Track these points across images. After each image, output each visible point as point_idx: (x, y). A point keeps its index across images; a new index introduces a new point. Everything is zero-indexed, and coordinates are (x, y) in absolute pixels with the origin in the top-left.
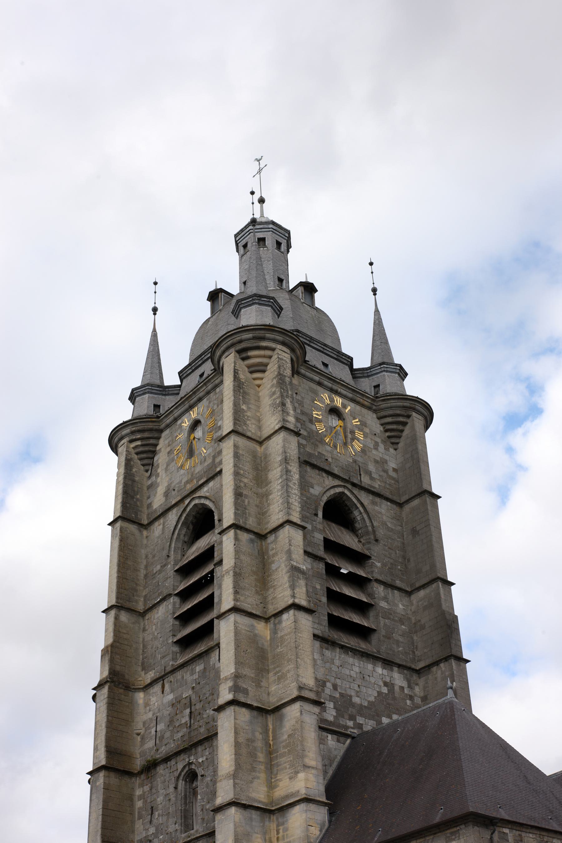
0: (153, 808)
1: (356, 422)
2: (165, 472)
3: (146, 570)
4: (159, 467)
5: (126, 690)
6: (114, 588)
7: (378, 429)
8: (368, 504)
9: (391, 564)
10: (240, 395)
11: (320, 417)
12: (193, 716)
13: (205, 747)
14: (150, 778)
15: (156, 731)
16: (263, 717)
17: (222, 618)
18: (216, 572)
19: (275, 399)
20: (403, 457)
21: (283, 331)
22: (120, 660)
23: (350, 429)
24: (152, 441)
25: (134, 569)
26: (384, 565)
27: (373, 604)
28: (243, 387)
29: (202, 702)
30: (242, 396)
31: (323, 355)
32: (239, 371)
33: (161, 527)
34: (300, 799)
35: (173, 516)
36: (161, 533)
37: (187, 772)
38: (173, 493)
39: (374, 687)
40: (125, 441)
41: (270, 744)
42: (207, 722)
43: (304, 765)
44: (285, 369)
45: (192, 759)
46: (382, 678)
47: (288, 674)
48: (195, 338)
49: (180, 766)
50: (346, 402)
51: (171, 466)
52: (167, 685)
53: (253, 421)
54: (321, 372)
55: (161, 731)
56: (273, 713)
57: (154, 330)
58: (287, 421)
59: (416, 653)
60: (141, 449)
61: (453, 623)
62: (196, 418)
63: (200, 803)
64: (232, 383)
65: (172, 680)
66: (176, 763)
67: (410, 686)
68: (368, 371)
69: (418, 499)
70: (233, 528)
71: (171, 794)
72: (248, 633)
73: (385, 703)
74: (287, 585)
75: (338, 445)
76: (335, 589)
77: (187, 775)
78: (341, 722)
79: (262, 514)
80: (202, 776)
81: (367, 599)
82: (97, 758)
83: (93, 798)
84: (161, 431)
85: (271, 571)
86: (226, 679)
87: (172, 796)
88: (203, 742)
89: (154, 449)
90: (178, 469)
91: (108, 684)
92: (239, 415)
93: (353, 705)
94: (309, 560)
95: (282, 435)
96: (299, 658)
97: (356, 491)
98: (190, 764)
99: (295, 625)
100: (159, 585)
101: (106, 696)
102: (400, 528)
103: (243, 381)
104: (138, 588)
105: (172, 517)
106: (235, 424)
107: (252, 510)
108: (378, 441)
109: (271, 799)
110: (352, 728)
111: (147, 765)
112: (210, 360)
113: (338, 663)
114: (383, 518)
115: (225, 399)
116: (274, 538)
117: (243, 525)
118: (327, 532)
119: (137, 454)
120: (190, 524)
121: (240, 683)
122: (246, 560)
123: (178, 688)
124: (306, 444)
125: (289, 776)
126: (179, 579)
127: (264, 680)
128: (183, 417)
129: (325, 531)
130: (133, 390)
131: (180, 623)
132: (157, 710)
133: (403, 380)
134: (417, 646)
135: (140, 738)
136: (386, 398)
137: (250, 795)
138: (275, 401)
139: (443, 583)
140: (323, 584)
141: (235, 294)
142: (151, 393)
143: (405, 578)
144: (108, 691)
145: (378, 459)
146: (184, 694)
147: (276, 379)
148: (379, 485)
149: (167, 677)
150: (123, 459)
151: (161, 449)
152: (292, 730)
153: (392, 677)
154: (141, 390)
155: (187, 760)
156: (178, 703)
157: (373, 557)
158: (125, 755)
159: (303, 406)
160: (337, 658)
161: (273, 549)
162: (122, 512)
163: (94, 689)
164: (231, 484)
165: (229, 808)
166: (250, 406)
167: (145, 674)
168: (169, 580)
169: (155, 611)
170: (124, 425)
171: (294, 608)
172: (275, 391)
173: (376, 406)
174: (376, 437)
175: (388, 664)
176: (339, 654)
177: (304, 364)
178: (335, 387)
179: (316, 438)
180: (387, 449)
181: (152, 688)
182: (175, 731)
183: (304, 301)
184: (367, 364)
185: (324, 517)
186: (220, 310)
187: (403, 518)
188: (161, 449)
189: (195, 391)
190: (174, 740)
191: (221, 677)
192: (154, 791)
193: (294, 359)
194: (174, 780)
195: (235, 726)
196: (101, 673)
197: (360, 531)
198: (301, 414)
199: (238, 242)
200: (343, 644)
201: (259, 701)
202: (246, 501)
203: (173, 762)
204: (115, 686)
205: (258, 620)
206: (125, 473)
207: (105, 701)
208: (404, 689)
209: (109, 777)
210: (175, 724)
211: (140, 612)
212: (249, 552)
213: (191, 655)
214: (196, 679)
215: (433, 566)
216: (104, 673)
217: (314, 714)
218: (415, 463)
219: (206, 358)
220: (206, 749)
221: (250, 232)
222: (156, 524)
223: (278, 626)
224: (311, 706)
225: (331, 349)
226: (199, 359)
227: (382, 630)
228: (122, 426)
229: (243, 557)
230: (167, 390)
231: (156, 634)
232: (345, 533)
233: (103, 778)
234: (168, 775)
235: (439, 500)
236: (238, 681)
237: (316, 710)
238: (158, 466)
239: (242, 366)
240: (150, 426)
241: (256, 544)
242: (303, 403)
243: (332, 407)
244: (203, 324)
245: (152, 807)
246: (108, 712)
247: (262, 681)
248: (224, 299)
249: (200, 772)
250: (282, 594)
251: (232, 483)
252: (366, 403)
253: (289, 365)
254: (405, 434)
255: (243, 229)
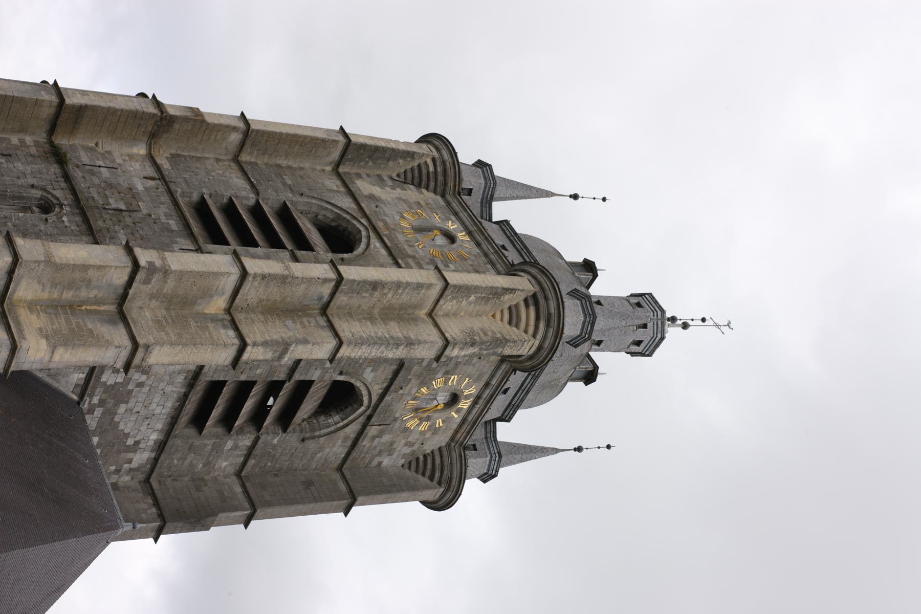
0: (9, 157)
1: (439, 423)
2: (397, 198)
3: (286, 167)
4: (403, 190)
5: (150, 135)
6: (270, 129)
7: (428, 448)
8: (346, 432)
9: (275, 455)
10: (486, 294)
11: (450, 383)
12: (117, 212)
13: (81, 226)
14: (45, 155)
15: (100, 166)
16: (115, 299)
17: (235, 258)
18: (283, 252)
19: (479, 334)
20: (393, 474)
21: (555, 348)
22: (186, 130)
23: (432, 416)
24: (432, 184)
25: (288, 153)
26: (274, 447)
27: (232, 433)
28: (494, 298)
29: (133, 225)
30: (485, 297)
31: (517, 389)
32: (514, 295)
33: (335, 188)
34: (15, 340)
35: (348, 204)
36: (328, 188)
37: (51, 201)
38: (373, 206)
39: (135, 429)
40: (435, 153)
41: (81, 306)
42: (110, 230)
43: (56, 347)
44: (511, 348)
45: (67, 209)
46: (144, 440)
47: (164, 333)
48: (544, 241)
49: (58, 193)
50: (463, 413)
51: (403, 205)
52: (154, 184)
53: (455, 307)
54: (500, 387)
55: (100, 172)
56: (119, 312)
57: (553, 195)
58: (454, 348)
59: (169, 479)
60: (424, 171)
61: (202, 525)
62: (458, 239)
63: (14, 215)
64: (500, 286)
65: (159, 190)
66: (62, 189)
67: (131, 470)
68: (492, 438)
69: (346, 491)
70: (338, 277)
71: (26, 180)
72: (215, 288)
73: (115, 441)
74: (268, 338)
75: (416, 402)
76: (253, 390)
77: (48, 201)
78: (98, 390)
79: (350, 314)
80: (46, 220)
81: (237, 426)
82: (73, 93)
83: (26, 85)
84: (443, 196)
85: (284, 319)
86: (163, 259)
87: (23, 181)
88: (86, 223)
89: (423, 185)
90: (400, 213)
91: (159, 114)
92: (464, 292)
93: (117, 405)
94: (290, 363)
95: (440, 343)
96: (182, 348)
97: (362, 419)
98: (61, 206)
99: (221, 345)
100: (269, 181)
101: (145, 110)
102: (314, 467)
103: (502, 299)
104: (266, 156)
105: (346, 203)
106: (455, 286)
107: (355, 301)
108: (415, 447)
109: (17, 304)
110: (90, 402)
111: (60, 153)
112: (523, 261)
113: (167, 390)
114: (327, 448)
115: (482, 276)
116: (322, 324)
117: (340, 289)
118: (320, 384)
119: (419, 166)
120: (337, 223)
121: (158, 275)
122: (299, 291)
123: (149, 196)
124: (423, 366)
125: (43, 328)
126: (275, 206)
127: (158, 303)
128: (459, 223)
129: (320, 382)
130: (490, 166)
131: (225, 203)
132: (125, 169)
133: (478, 478)
134: (177, 480)
135: (92, 146)
136: (463, 458)
137: (24, 280)
138: (477, 335)
139: (249, 515)
140: (262, 377)
141: (589, 290)
142: (485, 187)
143: (257, 470)
144: (151, 113)
145: (394, 446)
146: (142, 204)
147: (501, 338)
148: (365, 446)
149: (162, 184)
150: (415, 149)
151: (423, 194)
152: (97, 335)
153: (144, 451)
154: (490, 176)
155: (66, 203)
156: (132, 196)
157: (284, 435)
158: (74, 127)
159: (464, 365)
160: (174, 389)
161: (309, 322)
162: (356, 144)
163: (154, 96)
164: (388, 278)
165: (11, 253)
166: (473, 305)
167: (167, 158)
168: (274, 193)
169: (240, 174)
170: (453, 153)
171: (241, 345)
172: (488, 335)
173: (455, 446)
174: (419, 444)
175: (159, 446)
176: (178, 392)
177: (512, 369)
178: (481, 402)
179: (428, 377)
180: (404, 456)
181: (151, 165)
182: (100, 190)
183: (577, 370)
184: (500, 438)
185: (335, 383)
186: (573, 273)
187: (325, 471)
188: (423, 194)
189: (489, 240)
190: (89, 188)
191: (165, 253)
192: (30, 159)
193: (520, 359)
194: (43, 185)
195: (108, 266)
196: (172, 106)
197: (315, 421)
198: (457, 362)
199: (643, 297)
200: (190, 397)
201: (134, 296)
202: (367, 295)
203: (63, 185)
204: (156, 121)
205: (228, 301)
206: (399, 150)
207: (139, 108)
208: (128, 463)
209: (50, 106)
210: (108, 190)
211: (238, 157)
212: (308, 294)
213: (188, 215)
214: (160, 219)
215: (268, 504)
216: (172, 109)
217: (115, 362)
218: (387, 488)
219: (523, 253)
220: (78, 227)
221: (655, 311)
222: (339, 183)
223: (221, 323)
224: (125, 359)
225: (523, 398)
226: (522, 247)
227: (200, 442)
228: (452, 151)
229: (303, 287)
230: (487, 204)
231: (213, 174)
232: (315, 404)
233: (50, 99)
234: (48, 177)
235: (342, 514)
236: (161, 274)
237: (120, 364)
238: (404, 189)
239: (519, 298)
240: (450, 184)
241: (316, 302)
242: (468, 365)
243: (459, 397)
244: (559, 252)
245: (10, 156)
246: (127, 111)
247: (157, 301)
248: (585, 278)
249: (52, 217)
250: (257, 331)
251: (389, 279)
252: (459, 435)
253: (515, 353)
254: (420, 477)
255: (658, 303)
